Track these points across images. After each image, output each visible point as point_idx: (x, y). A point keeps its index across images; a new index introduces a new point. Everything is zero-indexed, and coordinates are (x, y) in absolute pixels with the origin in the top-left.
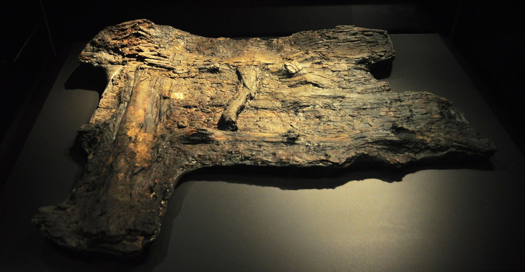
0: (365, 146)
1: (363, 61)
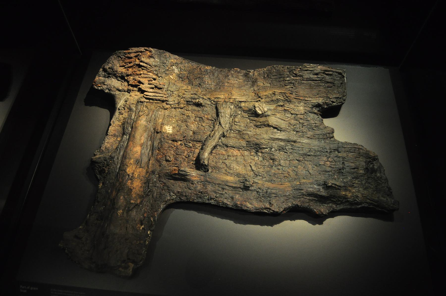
0: (300, 197)
1: (318, 105)
